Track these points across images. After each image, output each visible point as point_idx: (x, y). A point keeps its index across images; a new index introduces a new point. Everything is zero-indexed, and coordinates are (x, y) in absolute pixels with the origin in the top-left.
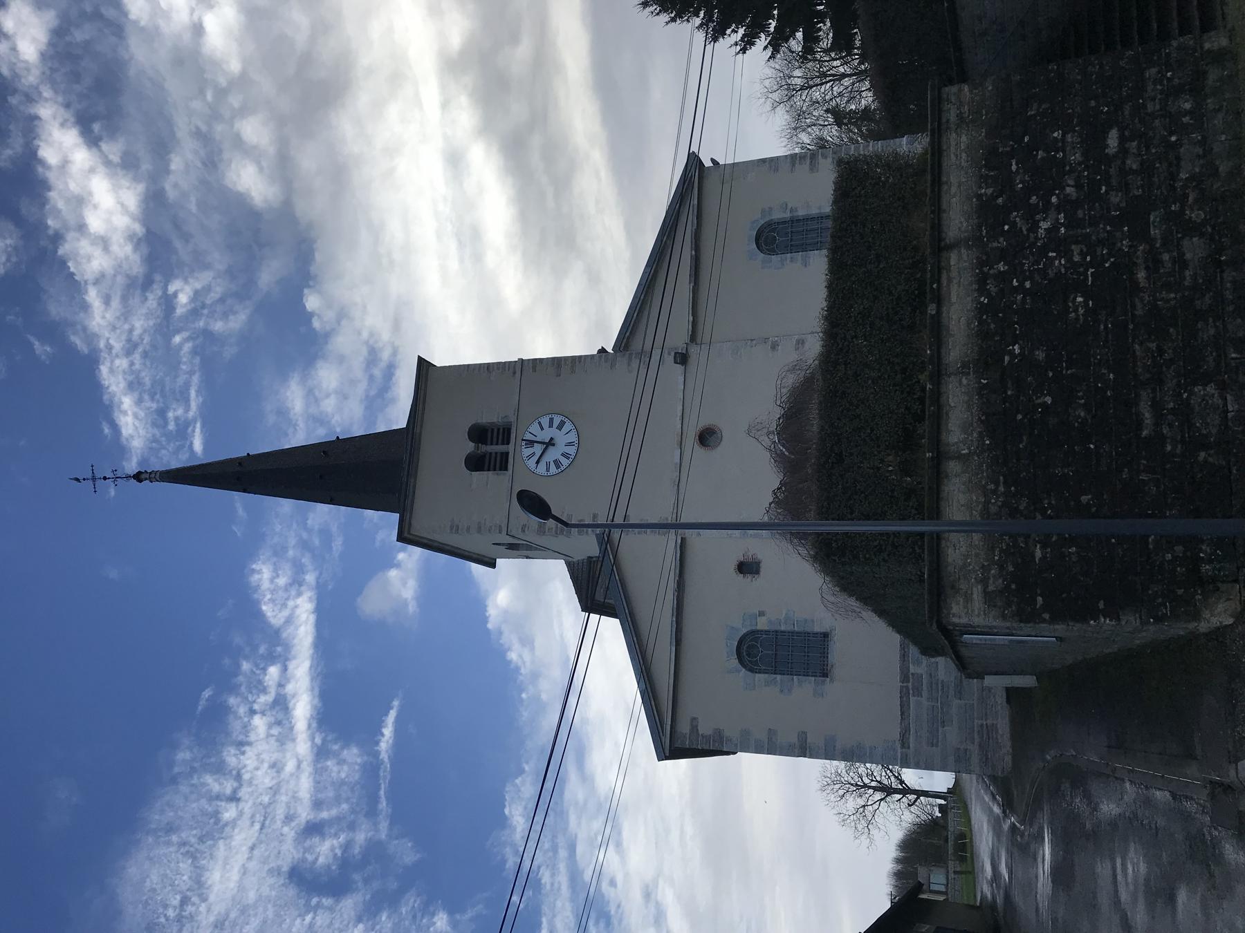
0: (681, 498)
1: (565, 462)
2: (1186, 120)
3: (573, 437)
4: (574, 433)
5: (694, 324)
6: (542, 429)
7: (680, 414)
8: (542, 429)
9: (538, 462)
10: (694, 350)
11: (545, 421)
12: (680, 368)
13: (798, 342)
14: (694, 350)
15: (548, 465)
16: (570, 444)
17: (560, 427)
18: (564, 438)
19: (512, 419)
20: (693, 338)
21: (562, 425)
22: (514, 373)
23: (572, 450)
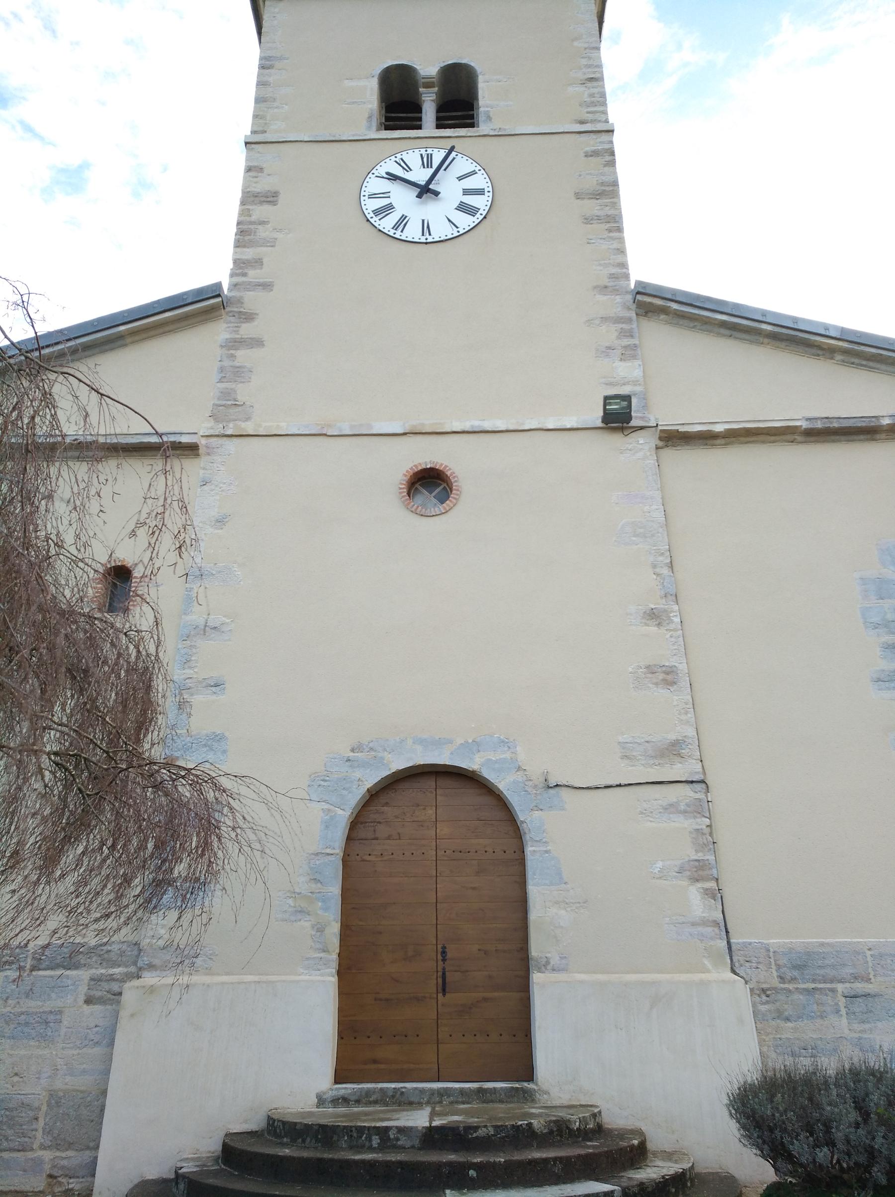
0: (89, 383)
1: (387, 224)
2: (472, 1173)
3: (441, 230)
4: (450, 232)
5: (706, 439)
6: (460, 178)
7: (488, 425)
8: (460, 178)
9: (392, 177)
10: (644, 443)
11: (479, 181)
12: (595, 416)
13: (670, 671)
14: (644, 443)
15: (385, 195)
16: (426, 227)
17: (464, 208)
18: (440, 217)
19: (484, 128)
20: (673, 439)
21: (470, 210)
22: (582, 122)
23: (413, 232)
